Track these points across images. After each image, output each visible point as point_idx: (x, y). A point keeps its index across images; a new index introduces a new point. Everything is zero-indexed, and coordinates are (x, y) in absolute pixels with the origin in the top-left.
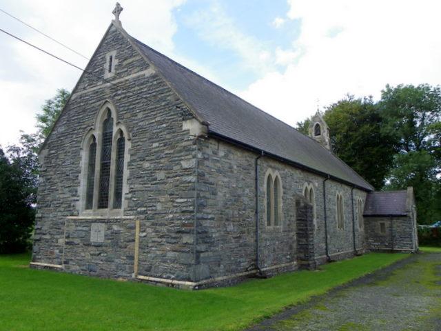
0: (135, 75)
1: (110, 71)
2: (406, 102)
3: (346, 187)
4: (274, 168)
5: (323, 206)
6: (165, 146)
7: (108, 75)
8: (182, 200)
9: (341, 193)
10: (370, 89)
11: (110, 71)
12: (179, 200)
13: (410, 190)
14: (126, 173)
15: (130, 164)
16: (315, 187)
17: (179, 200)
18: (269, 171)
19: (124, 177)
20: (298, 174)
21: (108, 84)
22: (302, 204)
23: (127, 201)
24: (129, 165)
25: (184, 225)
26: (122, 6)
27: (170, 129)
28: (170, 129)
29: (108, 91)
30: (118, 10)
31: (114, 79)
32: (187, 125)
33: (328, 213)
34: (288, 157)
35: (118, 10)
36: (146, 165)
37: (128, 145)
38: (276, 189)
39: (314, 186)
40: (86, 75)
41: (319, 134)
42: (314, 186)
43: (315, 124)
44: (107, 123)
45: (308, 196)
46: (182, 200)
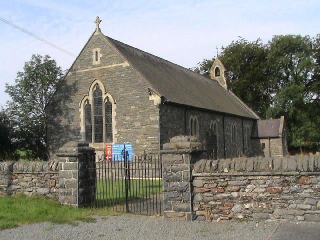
0: (115, 65)
1: (97, 60)
2: (289, 46)
3: (238, 120)
4: (194, 115)
5: (223, 134)
6: (139, 108)
7: (95, 63)
8: (152, 137)
9: (235, 124)
10: (262, 33)
11: (97, 60)
12: (150, 138)
13: (282, 118)
14: (114, 123)
15: (116, 118)
16: (219, 123)
17: (150, 138)
18: (191, 117)
19: (113, 125)
20: (207, 116)
21: (96, 69)
22: (210, 135)
23: (116, 138)
24: (116, 118)
25: (153, 150)
26: (100, 19)
27: (141, 99)
28: (141, 99)
29: (97, 73)
30: (99, 21)
31: (100, 66)
32: (152, 98)
33: (226, 138)
34: (201, 106)
35: (99, 21)
36: (128, 118)
37: (114, 107)
38: (195, 124)
39: (217, 121)
40: (163, 117)
41: (219, 75)
42: (217, 121)
43: (216, 67)
44: (97, 93)
45: (213, 129)
46: (152, 137)
